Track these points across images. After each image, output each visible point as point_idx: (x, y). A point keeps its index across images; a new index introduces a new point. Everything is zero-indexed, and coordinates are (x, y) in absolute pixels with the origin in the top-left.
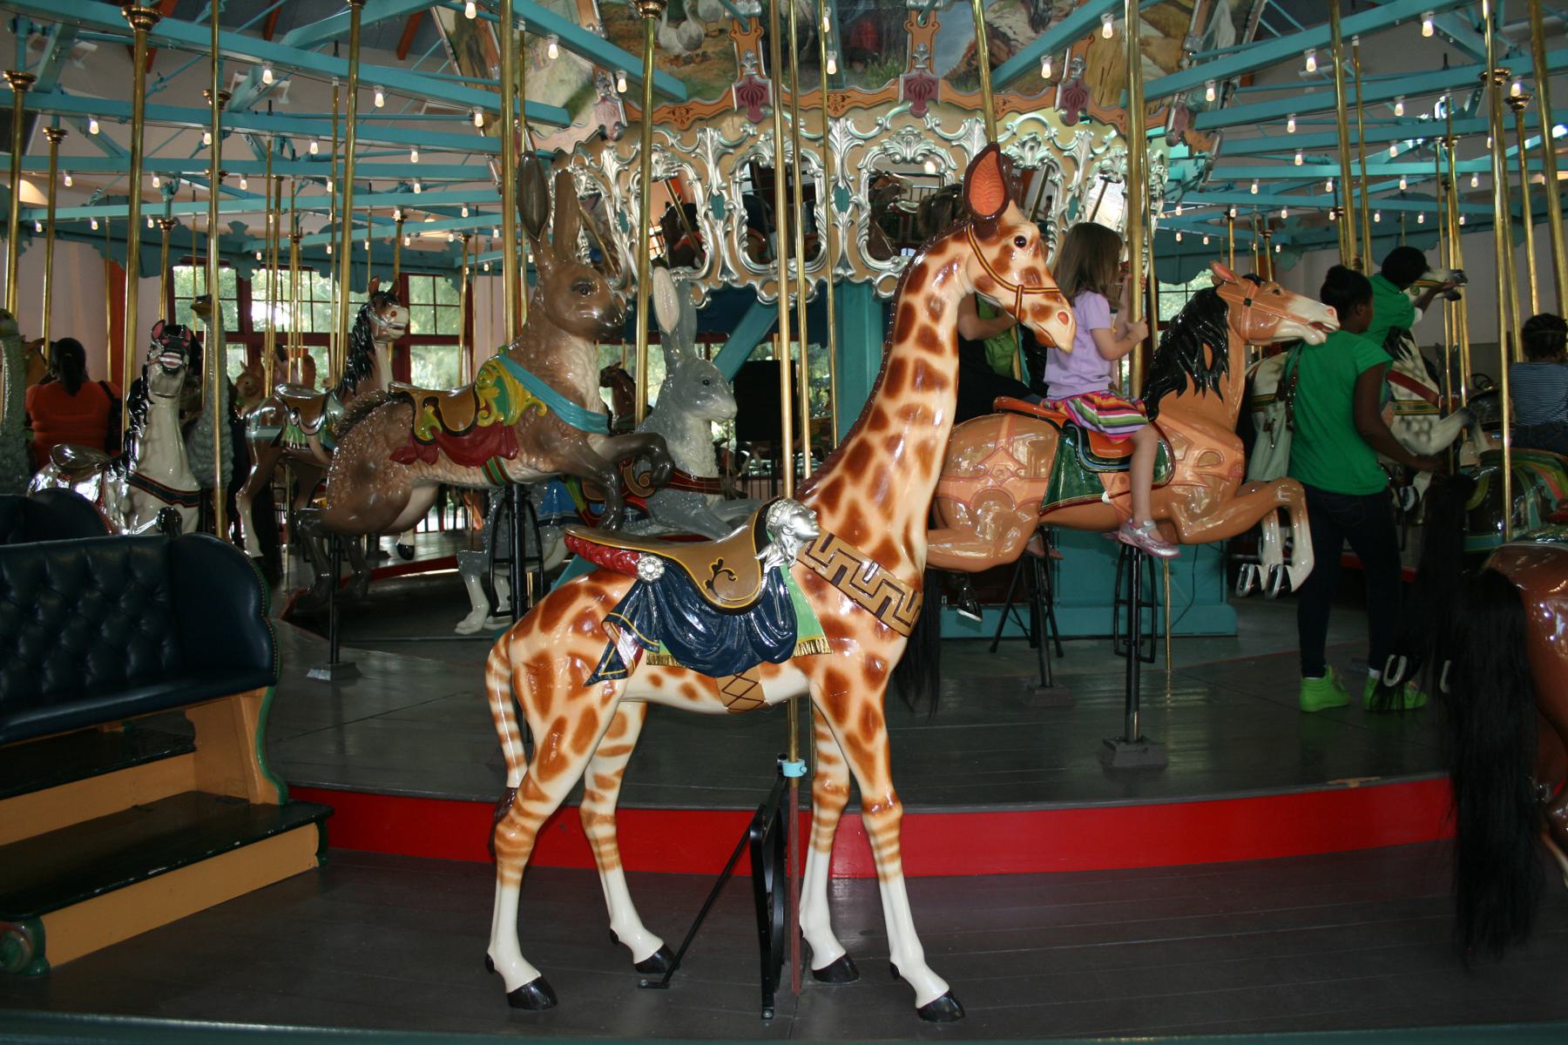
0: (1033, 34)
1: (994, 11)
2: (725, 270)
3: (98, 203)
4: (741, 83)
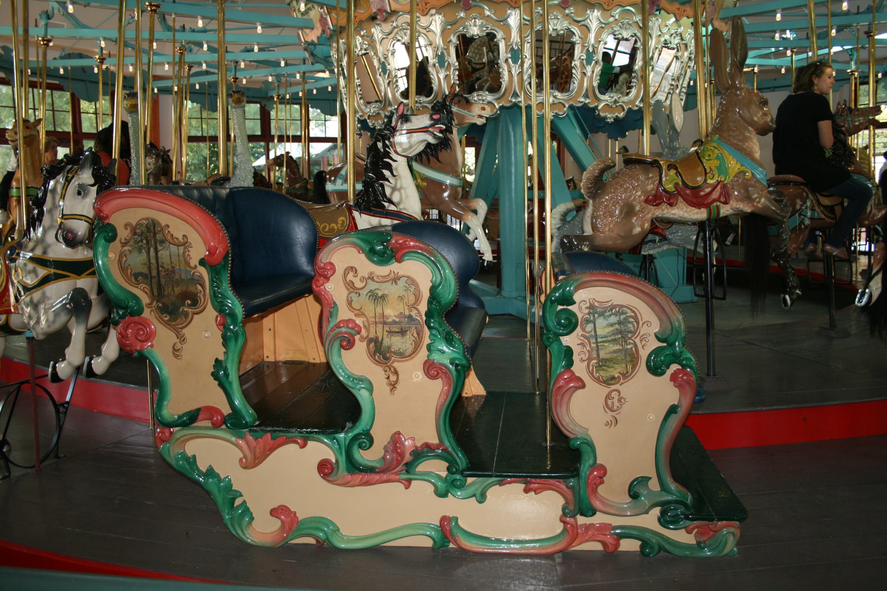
3: (62, 58)
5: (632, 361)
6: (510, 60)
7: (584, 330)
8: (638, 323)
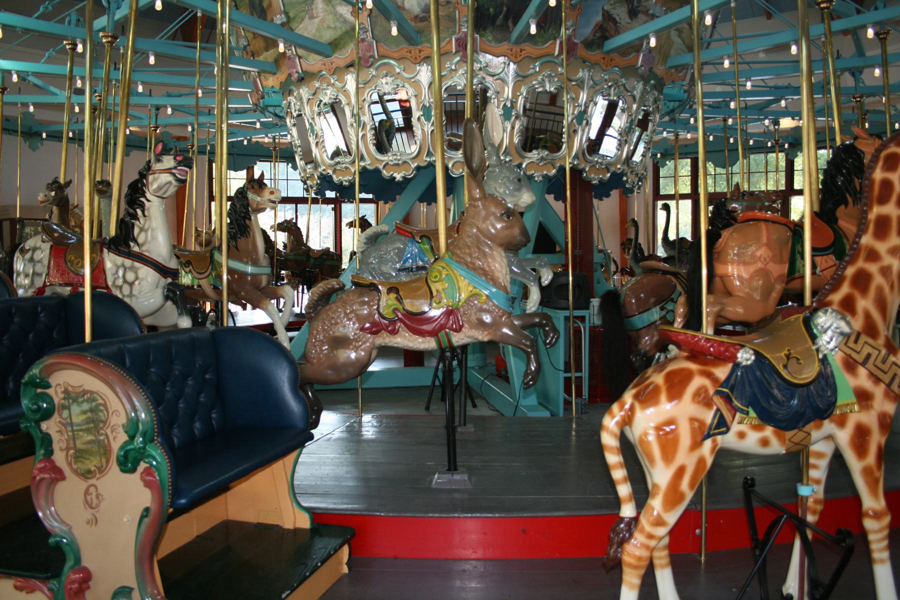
0: (629, 21)
1: (611, 5)
4: (460, 35)
5: (105, 454)
7: (61, 416)
8: (108, 412)
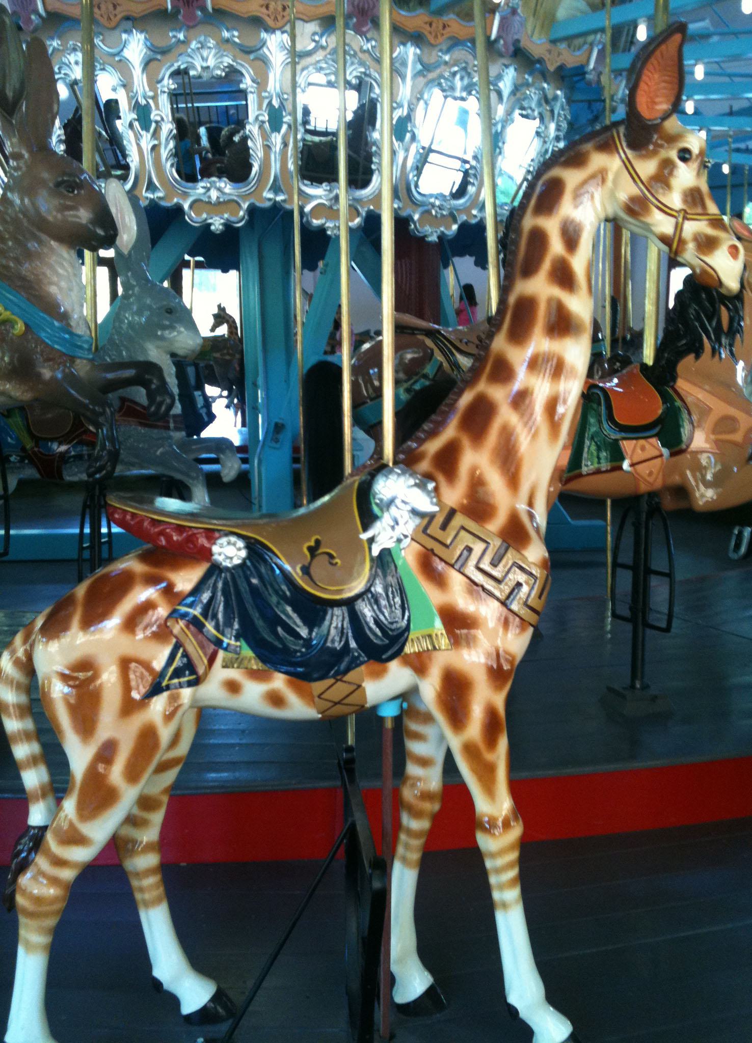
2: (151, 187)
6: (136, 124)
